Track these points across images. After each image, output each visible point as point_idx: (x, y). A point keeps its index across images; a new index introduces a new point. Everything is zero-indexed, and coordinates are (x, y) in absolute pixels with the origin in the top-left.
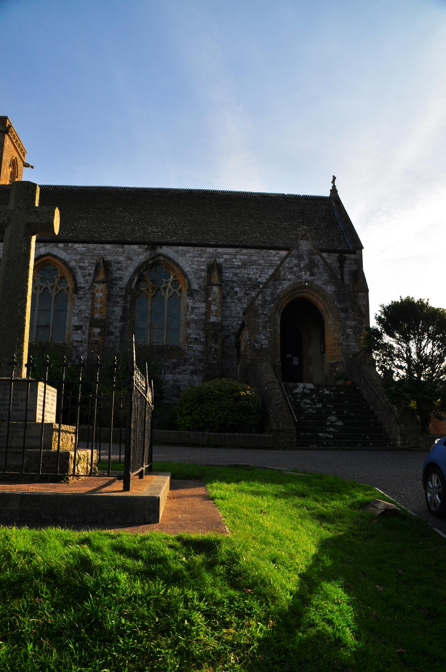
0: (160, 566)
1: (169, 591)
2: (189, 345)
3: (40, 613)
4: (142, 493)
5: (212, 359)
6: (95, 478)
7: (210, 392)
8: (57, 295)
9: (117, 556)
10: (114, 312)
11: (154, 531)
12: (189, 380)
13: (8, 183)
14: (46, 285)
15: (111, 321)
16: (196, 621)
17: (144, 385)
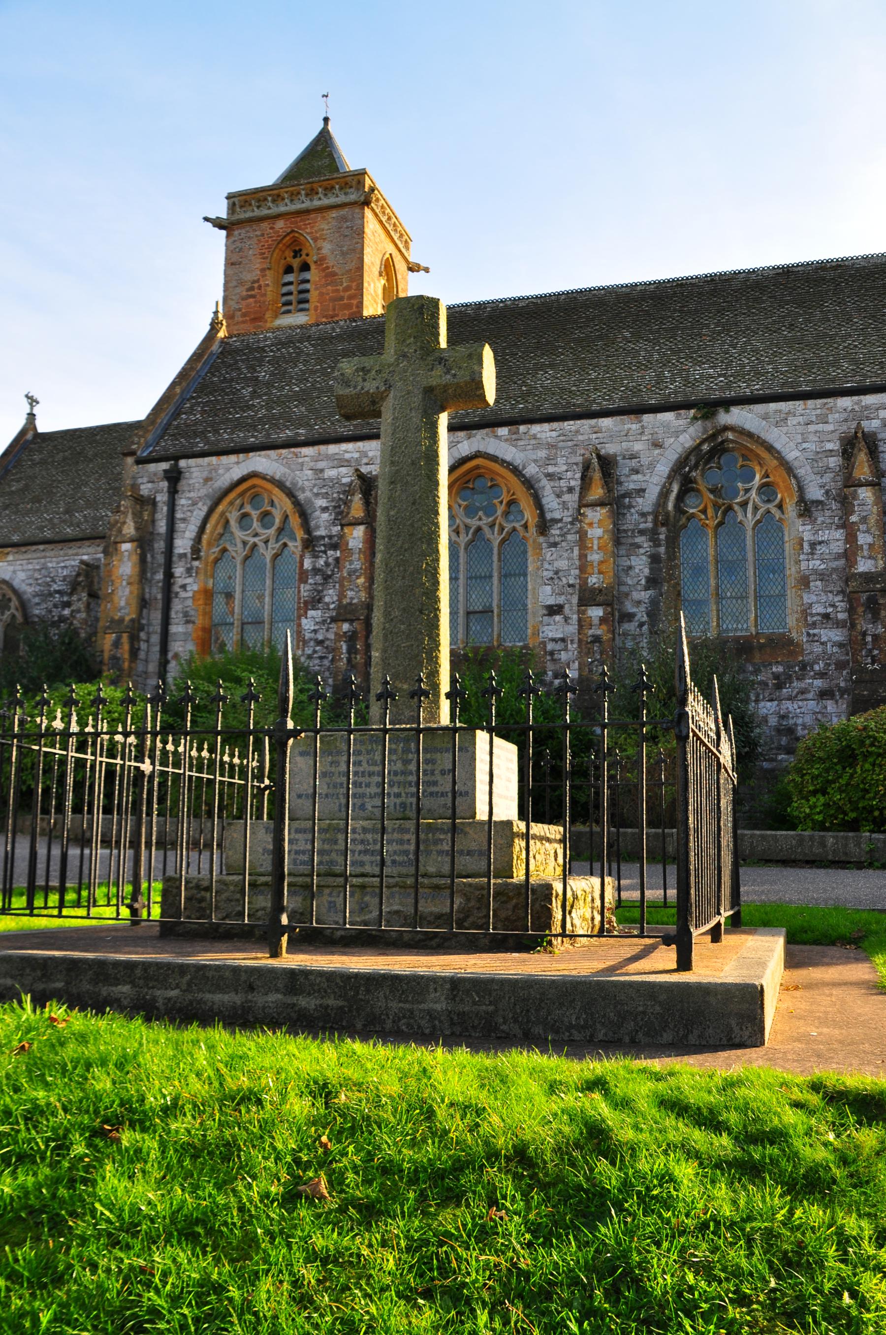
0: (773, 1151)
1: (798, 1213)
2: (811, 632)
3: (502, 1244)
4: (722, 974)
5: (869, 660)
6: (612, 940)
7: (869, 737)
8: (503, 541)
9: (670, 1121)
10: (630, 568)
11: (754, 1066)
12: (815, 713)
13: (380, 311)
14: (478, 523)
15: (624, 589)
16: (873, 1297)
17: (713, 726)
